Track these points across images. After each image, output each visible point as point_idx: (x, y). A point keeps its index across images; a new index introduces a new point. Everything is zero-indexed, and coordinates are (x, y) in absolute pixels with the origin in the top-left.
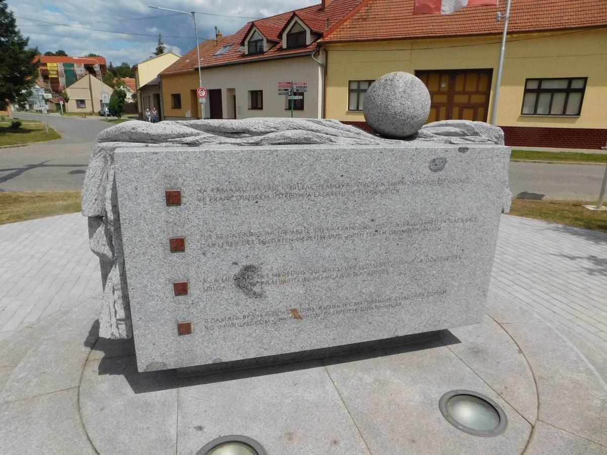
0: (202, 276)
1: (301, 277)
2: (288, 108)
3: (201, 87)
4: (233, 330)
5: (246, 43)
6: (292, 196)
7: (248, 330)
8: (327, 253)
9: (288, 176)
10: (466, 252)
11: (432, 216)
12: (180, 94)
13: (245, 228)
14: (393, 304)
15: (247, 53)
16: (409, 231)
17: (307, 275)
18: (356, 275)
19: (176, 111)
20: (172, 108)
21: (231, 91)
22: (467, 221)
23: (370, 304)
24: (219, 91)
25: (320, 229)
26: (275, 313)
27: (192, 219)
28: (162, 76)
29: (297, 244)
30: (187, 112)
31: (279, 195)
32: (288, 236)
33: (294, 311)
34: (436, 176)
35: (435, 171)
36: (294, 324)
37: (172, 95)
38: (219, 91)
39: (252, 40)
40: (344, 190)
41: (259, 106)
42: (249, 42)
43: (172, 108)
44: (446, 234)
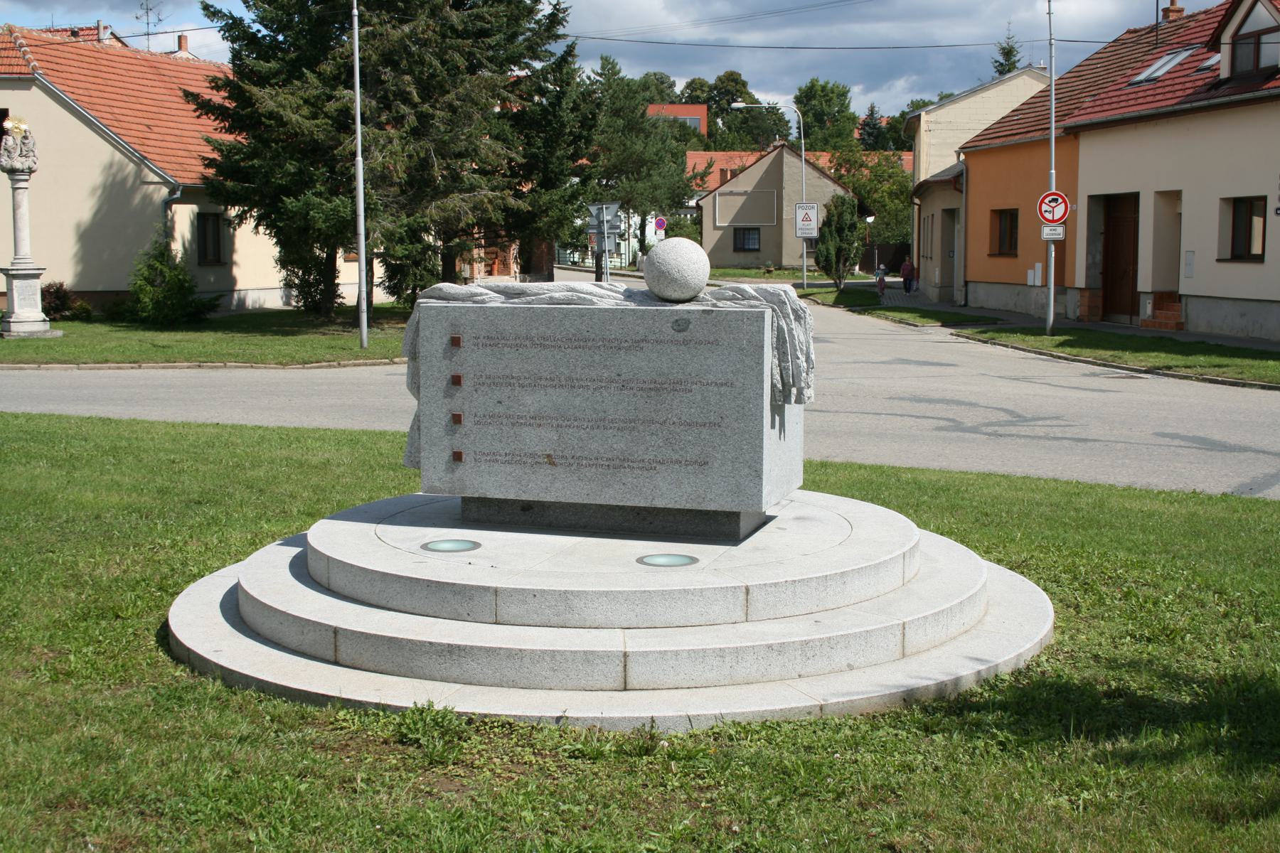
0: (474, 411)
1: (555, 423)
2: (1228, 256)
3: (1054, 190)
4: (496, 466)
5: (1226, 37)
6: (545, 347)
7: (508, 468)
8: (577, 401)
9: (542, 329)
10: (726, 420)
11: (680, 376)
12: (1016, 210)
13: (507, 372)
14: (650, 467)
15: (1224, 73)
16: (657, 390)
17: (560, 422)
18: (605, 428)
19: (1003, 262)
20: (989, 255)
21: (1173, 197)
22: (722, 385)
23: (619, 464)
24: (1132, 200)
25: (570, 379)
26: (533, 455)
27: (470, 360)
28: (970, 150)
29: (550, 390)
30: (1033, 268)
31: (534, 345)
32: (543, 382)
33: (549, 456)
34: (680, 336)
35: (679, 331)
36: (548, 470)
37: (994, 212)
38: (1132, 200)
39: (1244, 31)
40: (590, 344)
41: (1256, 249)
42: (1236, 39)
43: (989, 255)
44: (699, 397)
